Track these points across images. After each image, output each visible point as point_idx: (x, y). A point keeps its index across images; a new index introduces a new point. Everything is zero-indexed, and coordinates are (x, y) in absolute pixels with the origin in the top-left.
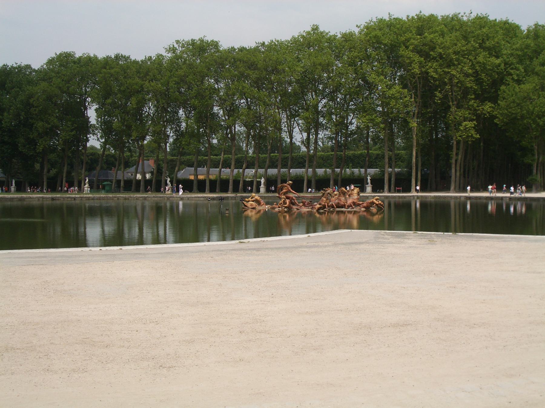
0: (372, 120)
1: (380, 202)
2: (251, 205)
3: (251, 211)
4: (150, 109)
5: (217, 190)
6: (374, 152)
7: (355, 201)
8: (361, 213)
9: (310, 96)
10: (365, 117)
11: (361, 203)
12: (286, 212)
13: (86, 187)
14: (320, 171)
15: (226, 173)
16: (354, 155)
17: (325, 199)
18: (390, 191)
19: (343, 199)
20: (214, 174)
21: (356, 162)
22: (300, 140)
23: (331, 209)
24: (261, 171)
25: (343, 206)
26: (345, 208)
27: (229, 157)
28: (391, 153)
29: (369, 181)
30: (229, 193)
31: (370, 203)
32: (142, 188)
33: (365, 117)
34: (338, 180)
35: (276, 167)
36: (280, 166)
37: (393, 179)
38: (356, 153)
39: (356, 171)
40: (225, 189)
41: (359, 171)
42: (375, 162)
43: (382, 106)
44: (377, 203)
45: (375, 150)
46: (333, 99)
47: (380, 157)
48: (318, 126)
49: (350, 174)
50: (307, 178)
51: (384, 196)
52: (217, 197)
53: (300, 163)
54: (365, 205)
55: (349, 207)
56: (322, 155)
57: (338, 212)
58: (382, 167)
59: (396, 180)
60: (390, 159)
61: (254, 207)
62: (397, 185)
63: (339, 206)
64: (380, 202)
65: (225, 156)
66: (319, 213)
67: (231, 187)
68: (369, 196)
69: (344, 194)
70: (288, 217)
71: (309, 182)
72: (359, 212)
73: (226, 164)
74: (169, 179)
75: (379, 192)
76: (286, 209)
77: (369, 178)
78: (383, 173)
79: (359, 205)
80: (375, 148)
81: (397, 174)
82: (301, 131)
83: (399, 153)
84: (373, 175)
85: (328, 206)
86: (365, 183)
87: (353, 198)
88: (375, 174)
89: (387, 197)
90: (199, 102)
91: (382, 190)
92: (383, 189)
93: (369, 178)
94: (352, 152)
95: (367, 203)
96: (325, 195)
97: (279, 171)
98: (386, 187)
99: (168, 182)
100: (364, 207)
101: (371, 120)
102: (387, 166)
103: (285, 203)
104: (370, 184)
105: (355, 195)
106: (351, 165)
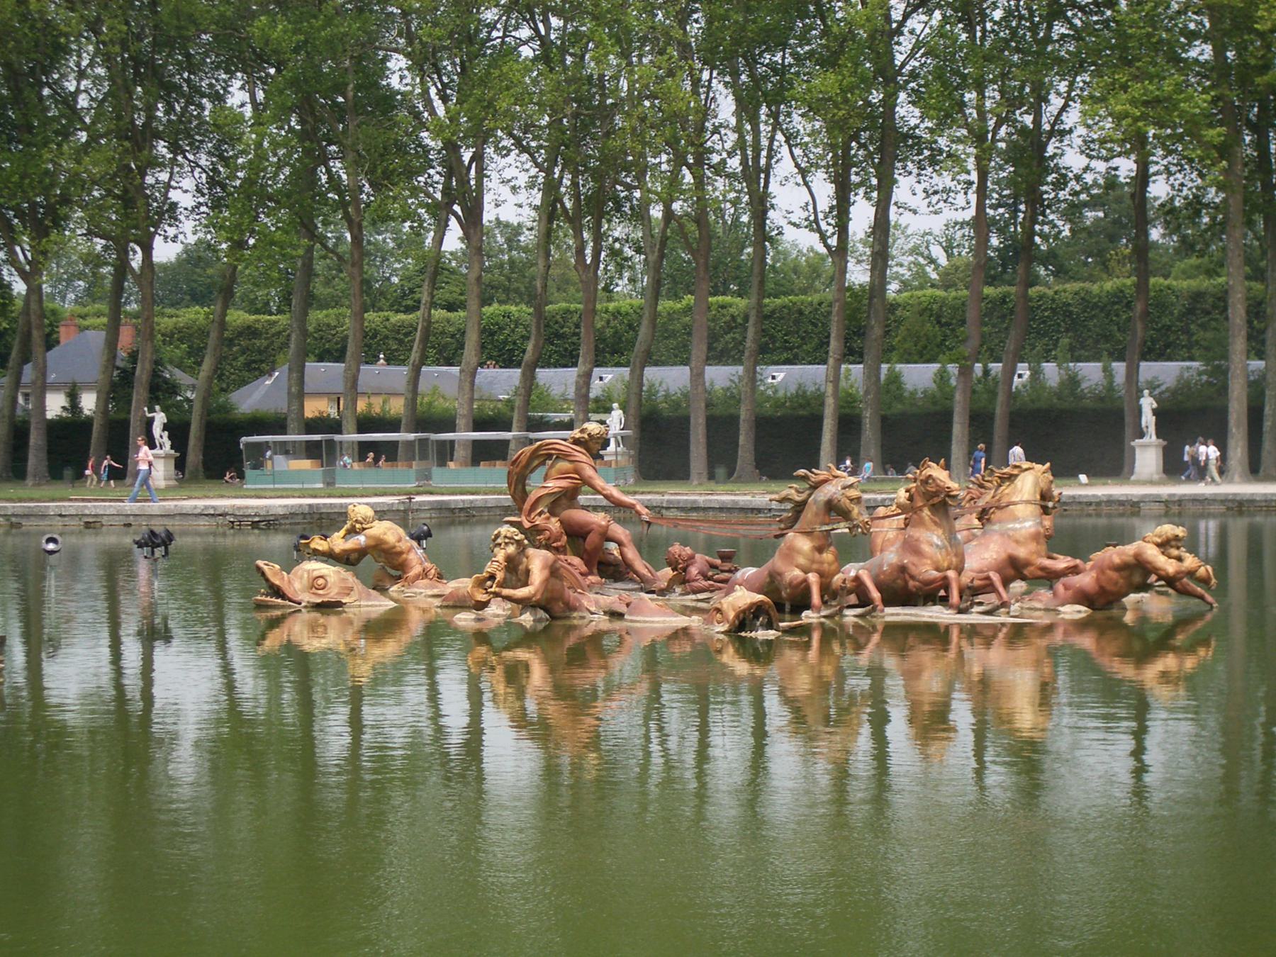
2: (315, 584)
3: (313, 628)
6: (1180, 282)
7: (1021, 553)
8: (1058, 637)
11: (1062, 563)
12: (528, 638)
13: (153, 461)
14: (918, 376)
16: (1086, 301)
17: (805, 544)
19: (931, 538)
21: (1089, 329)
23: (850, 616)
25: (932, 594)
26: (944, 601)
27: (507, 315)
28: (1258, 286)
29: (1148, 419)
32: (35, 459)
33: (1125, 88)
36: (698, 349)
38: (1095, 288)
39: (1091, 372)
41: (1107, 371)
42: (1187, 332)
43: (1216, 38)
44: (1170, 567)
45: (1187, 275)
47: (1208, 308)
48: (892, 146)
49: (1062, 383)
50: (839, 407)
52: (292, 515)
53: (791, 335)
54: (1086, 580)
55: (972, 592)
56: (934, 300)
57: (899, 635)
58: (1216, 353)
61: (332, 595)
63: (901, 590)
64: (1190, 561)
68: (1144, 499)
69: (940, 504)
70: (538, 675)
71: (849, 426)
72: (1049, 628)
74: (160, 418)
76: (527, 619)
77: (1148, 404)
78: (1220, 375)
79: (1050, 577)
82: (803, 172)
84: (1174, 392)
85: (829, 593)
86: (1128, 431)
88: (1183, 388)
89: (1239, 506)
90: (295, 32)
93: (1148, 404)
94: (1076, 286)
95: (1101, 570)
96: (808, 514)
97: (698, 376)
99: (157, 430)
100: (1082, 597)
101: (1157, 101)
102: (1239, 344)
104: (1151, 437)
105: (1020, 510)
106: (1065, 341)
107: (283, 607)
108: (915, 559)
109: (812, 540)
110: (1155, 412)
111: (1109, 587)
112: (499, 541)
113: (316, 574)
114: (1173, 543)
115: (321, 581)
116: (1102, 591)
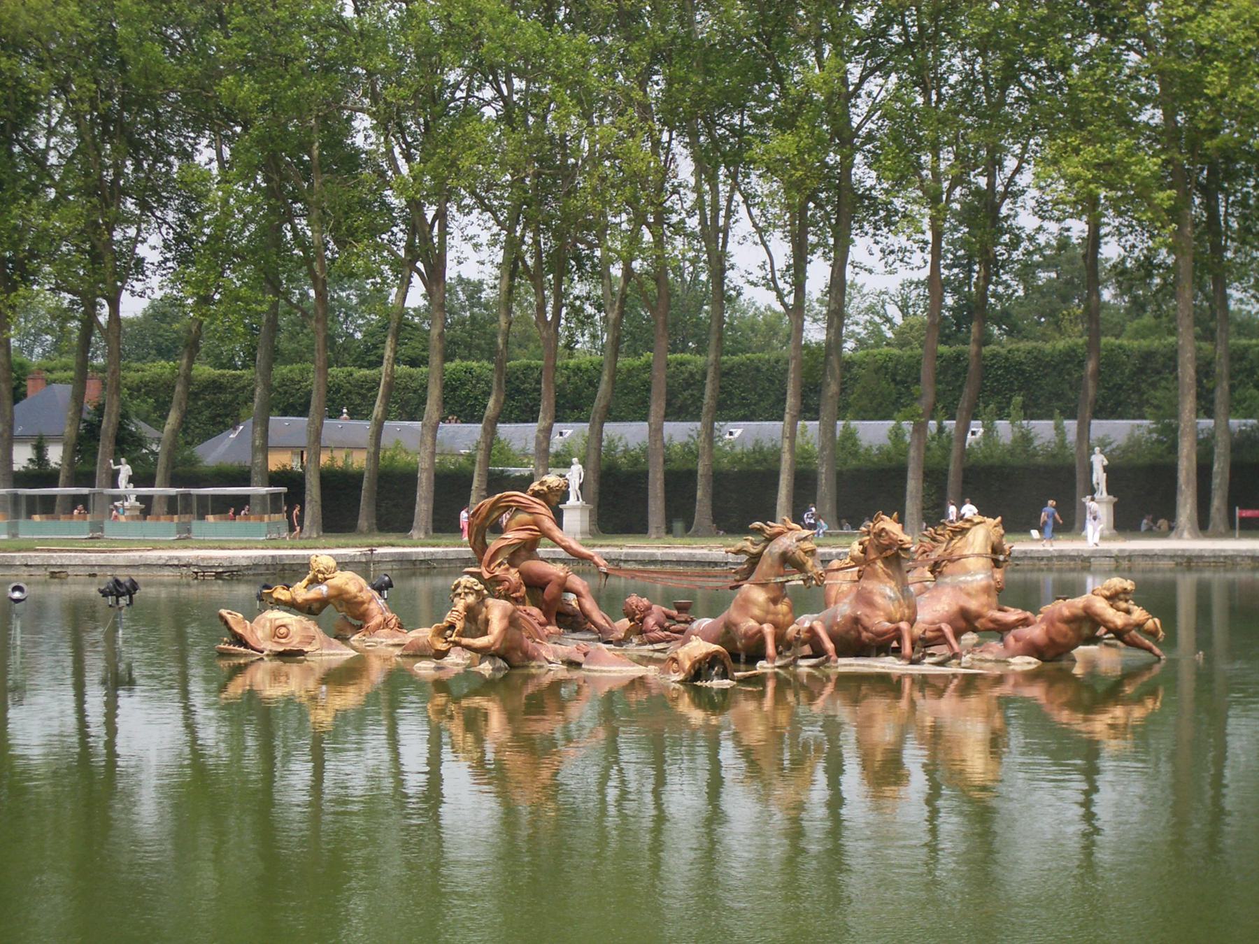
0: (1110, 170)
1: (1138, 614)
2: (277, 632)
3: (275, 676)
4: (53, 138)
5: (363, 523)
7: (973, 605)
9: (809, 70)
10: (1076, 151)
11: (1013, 615)
12: (486, 687)
14: (874, 433)
15: (406, 439)
16: (1038, 359)
17: (760, 595)
18: (1203, 526)
19: (884, 590)
20: (348, 443)
22: (757, 274)
23: (804, 666)
24: (568, 433)
25: (884, 645)
26: (897, 652)
27: (469, 371)
28: (1206, 346)
29: (1099, 476)
30: (416, 534)
31: (1073, 620)
33: (1076, 151)
34: (944, 473)
35: (638, 412)
36: (657, 406)
37: (1220, 467)
38: (1048, 347)
39: (1043, 430)
40: (395, 519)
42: (1138, 390)
44: (1119, 619)
45: (1138, 334)
46: (925, 78)
47: (1157, 367)
48: (850, 208)
50: (794, 463)
51: (1173, 556)
53: (749, 392)
54: (1036, 632)
55: (924, 644)
57: (852, 686)
59: (1237, 470)
60: (1205, 370)
61: (294, 643)
62: (1236, 498)
63: (854, 642)
65: (450, 366)
66: (704, 700)
67: (423, 507)
70: (496, 723)
72: (1000, 680)
73: (408, 404)
75: (1152, 533)
76: (486, 668)
77: (1099, 461)
78: (1170, 436)
80: (1136, 324)
81: (1240, 444)
82: (760, 231)
83: (1246, 349)
84: (1125, 451)
85: (783, 643)
86: (1080, 487)
87: (957, 587)
88: (1134, 444)
89: (1189, 562)
90: (262, 91)
91: (1163, 523)
92: (1171, 515)
93: (1099, 461)
94: (1029, 345)
96: (764, 566)
97: (656, 432)
98: (1186, 509)
100: (1033, 649)
102: (1188, 403)
103: (475, 621)
104: (1102, 493)
105: (972, 563)
106: (1018, 399)
107: (246, 655)
108: (868, 611)
109: (767, 592)
110: (1106, 469)
111: (1059, 639)
112: (459, 591)
113: (278, 623)
114: (1122, 596)
115: (283, 630)
116: (1052, 642)
